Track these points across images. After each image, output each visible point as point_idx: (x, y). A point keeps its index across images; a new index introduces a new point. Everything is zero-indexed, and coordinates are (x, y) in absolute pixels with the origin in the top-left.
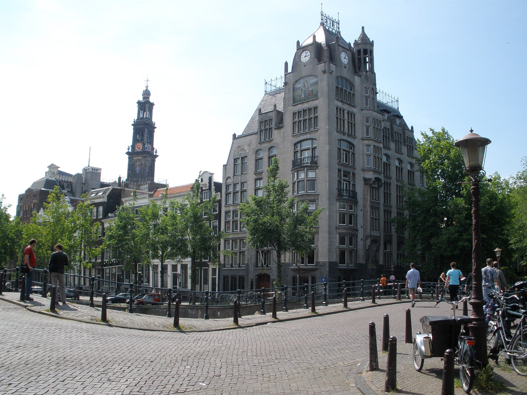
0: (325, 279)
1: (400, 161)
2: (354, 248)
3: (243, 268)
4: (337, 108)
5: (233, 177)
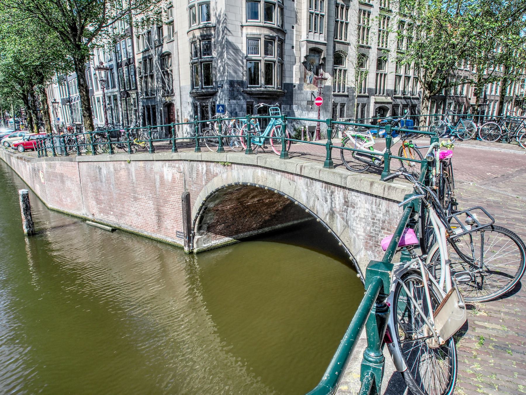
0: (223, 108)
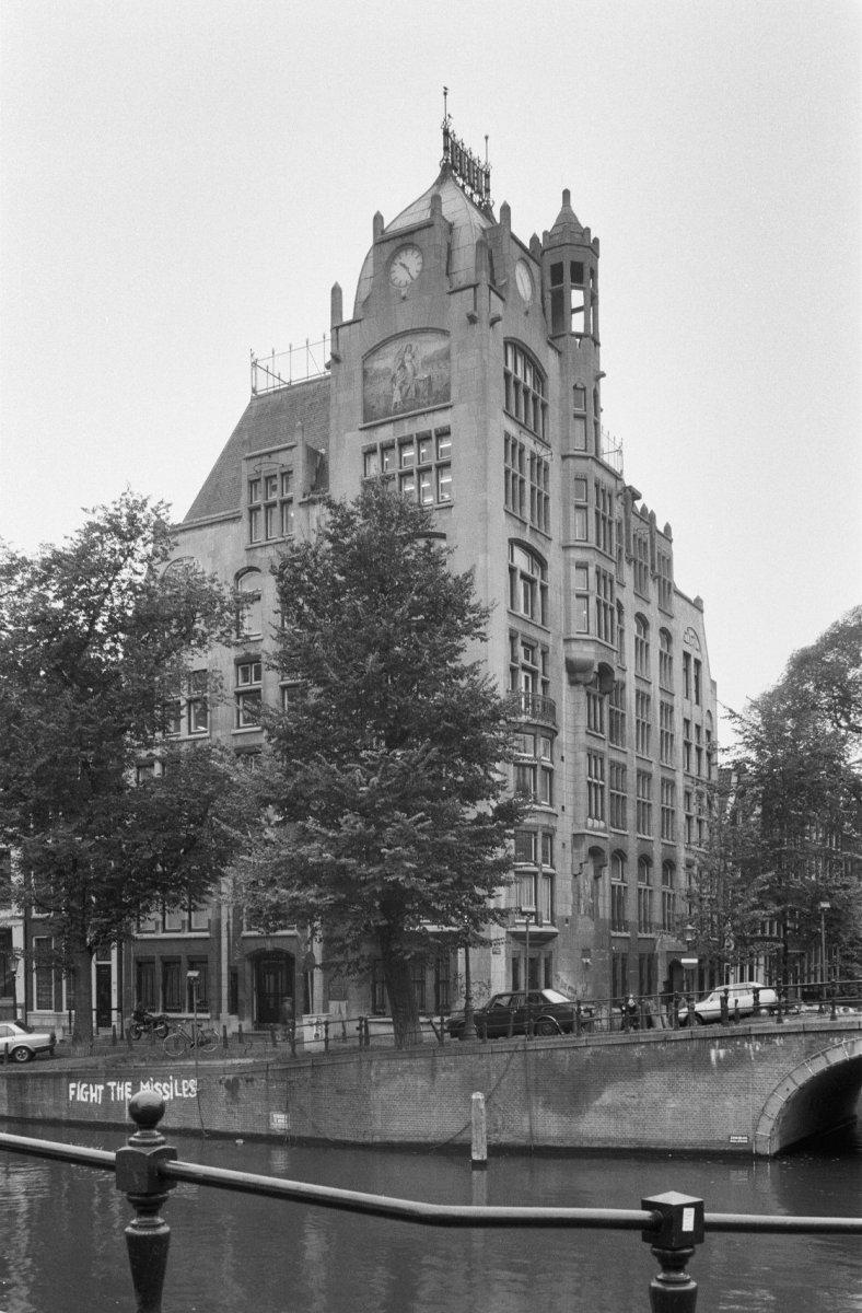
1: (642, 621)
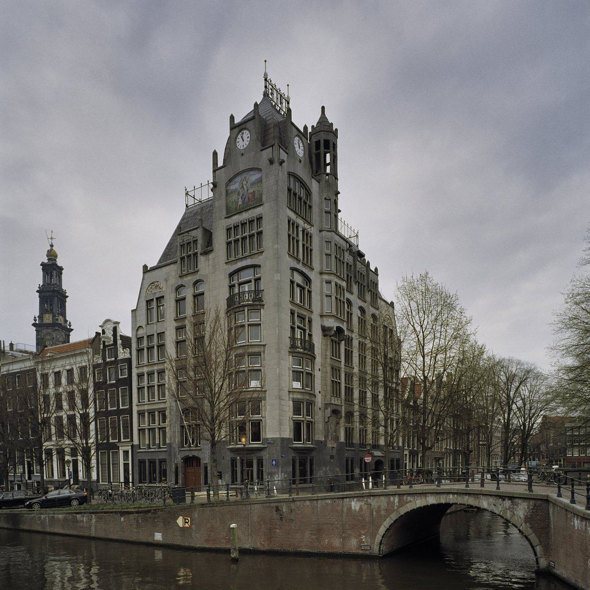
1: (362, 309)
2: (312, 420)
3: (163, 450)
4: (289, 221)
5: (146, 326)
